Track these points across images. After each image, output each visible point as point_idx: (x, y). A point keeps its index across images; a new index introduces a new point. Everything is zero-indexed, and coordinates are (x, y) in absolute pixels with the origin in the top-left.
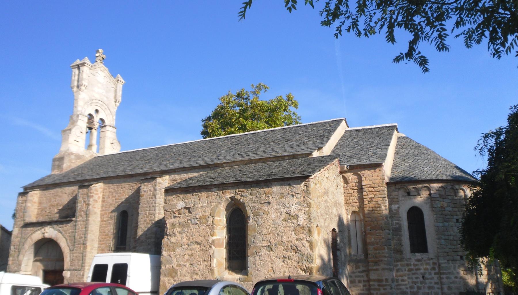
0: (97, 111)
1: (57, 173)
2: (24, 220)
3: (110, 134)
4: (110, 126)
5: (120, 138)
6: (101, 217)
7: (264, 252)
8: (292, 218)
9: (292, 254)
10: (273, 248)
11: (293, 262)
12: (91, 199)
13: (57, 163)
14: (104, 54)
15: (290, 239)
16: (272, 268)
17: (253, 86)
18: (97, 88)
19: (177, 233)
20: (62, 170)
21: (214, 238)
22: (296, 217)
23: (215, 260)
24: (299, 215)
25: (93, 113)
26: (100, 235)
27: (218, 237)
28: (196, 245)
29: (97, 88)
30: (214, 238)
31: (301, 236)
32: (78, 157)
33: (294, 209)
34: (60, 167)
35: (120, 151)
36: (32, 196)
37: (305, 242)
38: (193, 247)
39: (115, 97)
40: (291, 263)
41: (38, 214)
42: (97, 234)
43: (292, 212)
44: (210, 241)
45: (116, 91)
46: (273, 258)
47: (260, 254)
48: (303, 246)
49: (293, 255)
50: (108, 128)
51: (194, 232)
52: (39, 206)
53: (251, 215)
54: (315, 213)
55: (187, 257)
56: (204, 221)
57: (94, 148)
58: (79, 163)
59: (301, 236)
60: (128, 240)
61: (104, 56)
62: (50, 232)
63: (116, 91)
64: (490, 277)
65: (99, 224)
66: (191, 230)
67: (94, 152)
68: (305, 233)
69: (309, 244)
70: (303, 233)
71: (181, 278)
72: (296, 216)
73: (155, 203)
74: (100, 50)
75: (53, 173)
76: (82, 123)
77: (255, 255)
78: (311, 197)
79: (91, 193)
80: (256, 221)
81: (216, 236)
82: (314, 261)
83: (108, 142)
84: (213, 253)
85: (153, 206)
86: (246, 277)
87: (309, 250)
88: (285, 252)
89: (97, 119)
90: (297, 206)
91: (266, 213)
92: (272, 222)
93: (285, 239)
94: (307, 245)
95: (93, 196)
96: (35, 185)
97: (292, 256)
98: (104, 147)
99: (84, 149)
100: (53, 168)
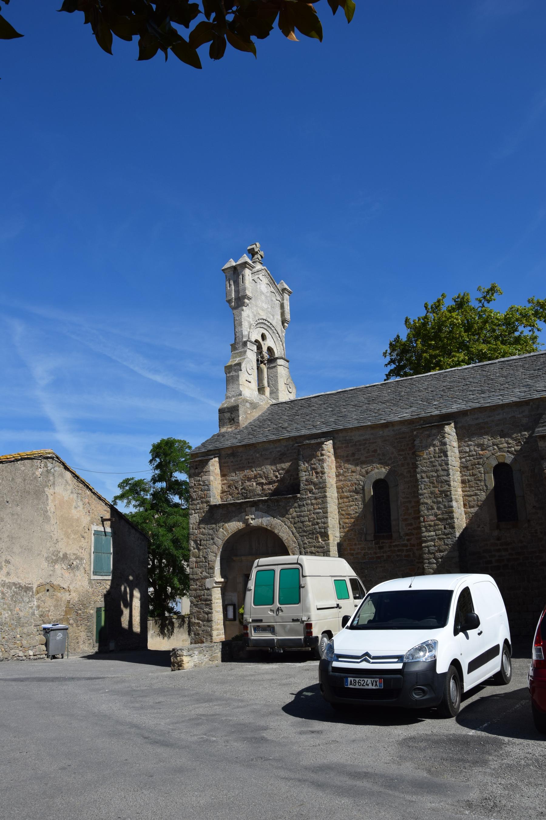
2: (208, 502)
3: (282, 370)
5: (296, 379)
6: (338, 492)
17: (479, 289)
20: (239, 426)
26: (340, 519)
35: (296, 397)
36: (213, 465)
39: (283, 314)
42: (337, 517)
45: (282, 306)
50: (280, 362)
52: (222, 480)
60: (393, 523)
61: (262, 253)
63: (282, 306)
64: (273, 463)
65: (336, 501)
73: (447, 464)
74: (258, 244)
75: (223, 430)
83: (282, 386)
85: (444, 470)
96: (210, 447)
98: (277, 390)
100: (222, 422)
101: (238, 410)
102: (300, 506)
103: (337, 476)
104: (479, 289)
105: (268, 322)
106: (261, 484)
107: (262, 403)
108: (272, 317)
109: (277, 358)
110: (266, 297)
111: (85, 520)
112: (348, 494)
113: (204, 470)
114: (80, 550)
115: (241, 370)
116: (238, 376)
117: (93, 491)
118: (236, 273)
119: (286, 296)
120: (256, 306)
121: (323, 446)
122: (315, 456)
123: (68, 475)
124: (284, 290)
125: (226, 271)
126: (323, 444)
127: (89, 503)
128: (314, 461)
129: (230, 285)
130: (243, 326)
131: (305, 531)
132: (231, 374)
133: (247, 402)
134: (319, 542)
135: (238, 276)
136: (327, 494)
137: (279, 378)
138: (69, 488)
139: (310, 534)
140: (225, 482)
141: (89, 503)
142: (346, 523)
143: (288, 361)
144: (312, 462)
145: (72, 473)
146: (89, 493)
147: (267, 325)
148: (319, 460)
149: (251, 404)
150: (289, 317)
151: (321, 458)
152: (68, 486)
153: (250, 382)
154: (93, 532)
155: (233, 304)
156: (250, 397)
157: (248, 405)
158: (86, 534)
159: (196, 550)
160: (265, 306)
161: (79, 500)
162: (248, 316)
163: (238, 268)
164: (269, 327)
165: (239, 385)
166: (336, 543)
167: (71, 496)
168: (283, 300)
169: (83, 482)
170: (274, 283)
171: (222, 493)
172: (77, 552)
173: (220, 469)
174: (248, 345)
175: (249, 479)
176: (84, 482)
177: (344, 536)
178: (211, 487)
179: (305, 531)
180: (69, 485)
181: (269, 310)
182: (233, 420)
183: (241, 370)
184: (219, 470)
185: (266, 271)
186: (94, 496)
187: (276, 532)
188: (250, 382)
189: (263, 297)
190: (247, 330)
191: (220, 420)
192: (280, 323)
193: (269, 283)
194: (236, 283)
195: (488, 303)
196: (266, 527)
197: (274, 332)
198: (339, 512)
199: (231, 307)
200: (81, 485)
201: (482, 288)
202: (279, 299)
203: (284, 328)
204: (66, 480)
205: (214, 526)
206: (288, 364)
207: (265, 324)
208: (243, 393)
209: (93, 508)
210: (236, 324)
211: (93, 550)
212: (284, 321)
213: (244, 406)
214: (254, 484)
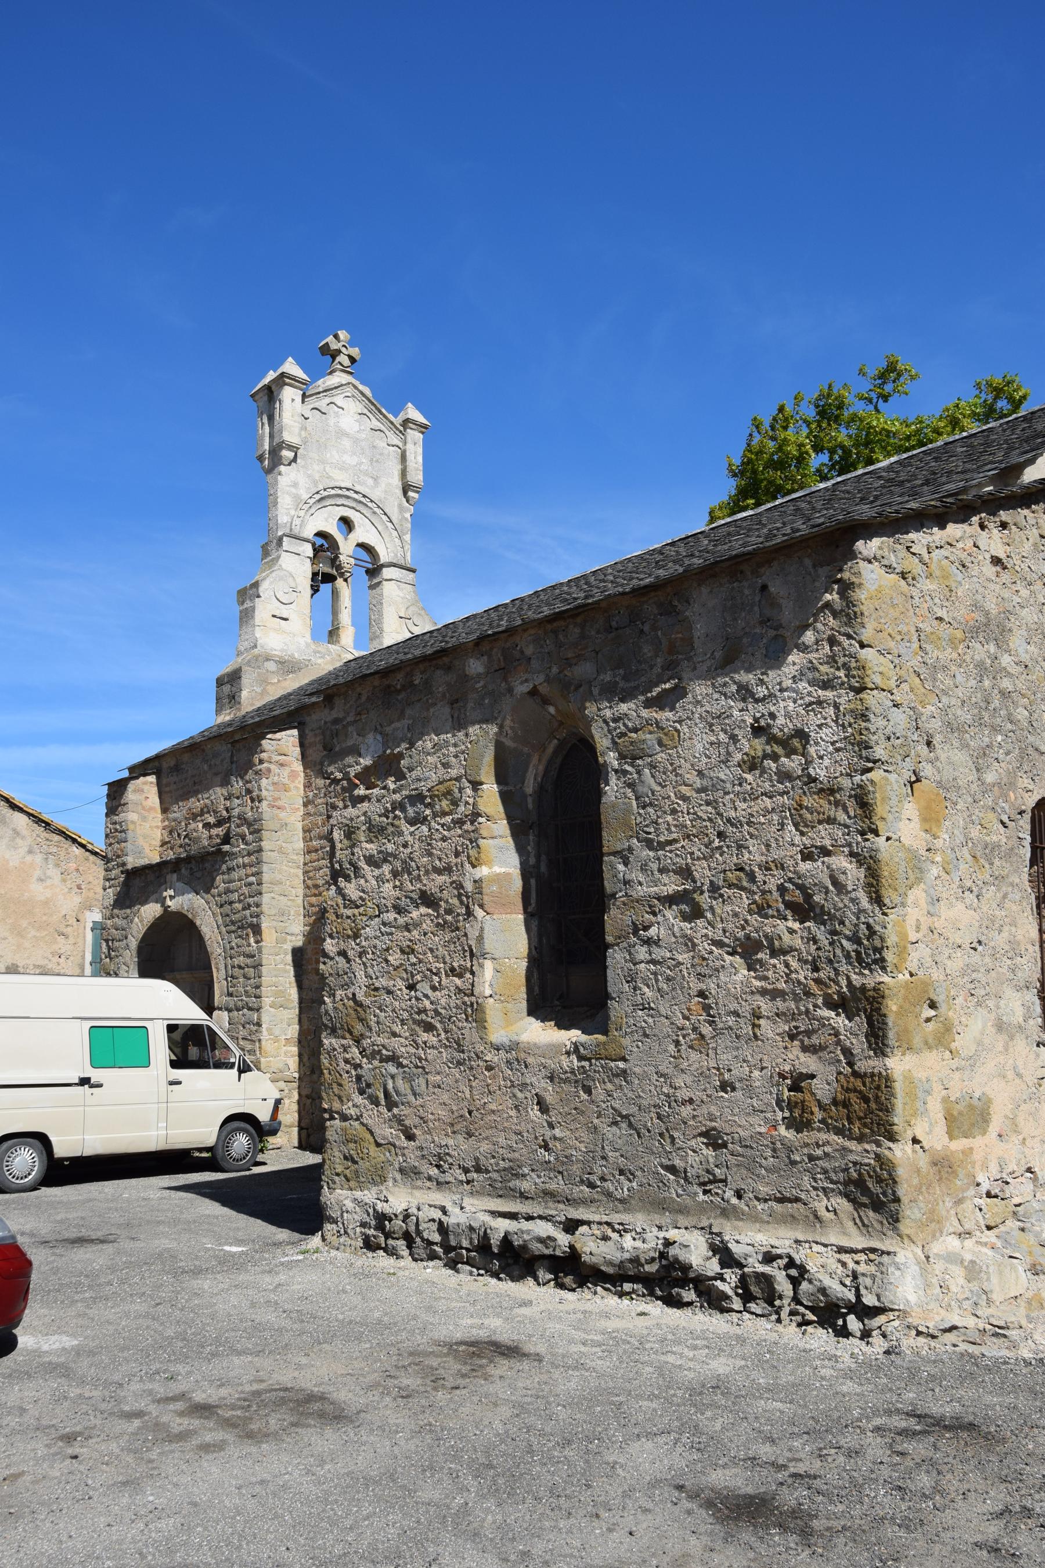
0: (347, 523)
1: (228, 718)
4: (395, 565)
7: (669, 923)
8: (779, 750)
9: (787, 930)
10: (704, 900)
11: (794, 964)
12: (264, 782)
13: (226, 689)
14: (352, 343)
15: (776, 854)
16: (701, 994)
18: (342, 448)
19: (362, 864)
20: (239, 710)
21: (483, 871)
22: (798, 740)
23: (488, 965)
24: (811, 730)
25: (332, 528)
27: (497, 869)
28: (423, 910)
29: (342, 448)
30: (483, 871)
31: (823, 835)
32: (288, 666)
33: (786, 713)
34: (233, 699)
36: (140, 791)
37: (841, 862)
38: (415, 914)
39: (404, 473)
40: (781, 967)
41: (164, 844)
43: (781, 721)
44: (469, 886)
45: (403, 458)
46: (704, 946)
47: (653, 932)
48: (835, 882)
49: (791, 931)
50: (387, 573)
51: (415, 855)
52: (163, 821)
53: (611, 758)
54: (900, 719)
55: (395, 958)
56: (445, 804)
57: (347, 636)
58: (292, 683)
59: (823, 835)
61: (355, 352)
62: (181, 901)
63: (403, 458)
66: (405, 846)
67: (349, 648)
68: (842, 817)
69: (862, 873)
70: (831, 821)
71: (380, 1040)
72: (796, 743)
74: (343, 335)
76: (296, 565)
77: (633, 939)
78: (866, 635)
79: (261, 762)
80: (631, 785)
81: (489, 864)
82: (890, 956)
84: (480, 939)
86: (601, 1038)
87: (865, 903)
88: (754, 920)
89: (347, 548)
90: (803, 686)
91: (668, 739)
92: (692, 777)
93: (754, 855)
94: (853, 873)
95: (269, 770)
97: (786, 938)
98: (382, 630)
99: (308, 638)
101: (240, 678)
102: (230, 870)
103: (305, 805)
104: (862, 373)
105: (356, 492)
106: (207, 826)
107: (319, 661)
108: (370, 482)
109: (383, 566)
110: (356, 441)
111: (69, 903)
112: (318, 842)
113: (122, 802)
114: (56, 959)
115: (259, 596)
116: (253, 608)
117: (90, 847)
118: (270, 394)
119: (415, 436)
120: (323, 462)
121: (263, 742)
122: (250, 765)
123: (21, 819)
124: (406, 422)
125: (257, 397)
126: (264, 738)
127: (77, 870)
128: (250, 775)
129: (263, 424)
130: (279, 505)
131: (233, 923)
132: (245, 606)
133: (268, 660)
134: (249, 945)
135: (275, 403)
136: (263, 844)
137: (385, 605)
138: (23, 845)
139: (239, 928)
140: (166, 823)
141: (77, 870)
142: (312, 905)
143: (414, 571)
144: (247, 777)
145: (29, 815)
146: (76, 851)
147: (355, 500)
148: (256, 773)
149: (281, 662)
150: (421, 477)
151: (259, 767)
152: (19, 841)
153: (286, 619)
154: (90, 925)
155: (266, 462)
156: (282, 650)
157: (271, 666)
158: (69, 929)
159: (108, 960)
160: (351, 460)
161: (50, 866)
162: (295, 485)
163: (274, 388)
164: (360, 502)
165: (254, 626)
166: (288, 947)
167: (29, 858)
168: (405, 443)
169: (61, 833)
170: (380, 411)
171: (162, 846)
172: (46, 962)
173: (160, 798)
174: (284, 544)
175: (194, 817)
176: (64, 833)
177: (310, 933)
178: (130, 835)
179: (233, 923)
180: (23, 838)
181: (363, 467)
182: (234, 697)
183: (259, 596)
184: (158, 800)
185: (355, 387)
186: (92, 858)
187: (198, 923)
188: (286, 619)
189: (346, 443)
190: (288, 514)
191: (218, 699)
192: (399, 492)
193: (366, 411)
194: (271, 419)
195: (886, 401)
196: (186, 913)
197: (375, 513)
198: (304, 881)
199: (263, 468)
200: (57, 838)
201: (866, 369)
202: (396, 442)
203: (408, 501)
204: (14, 830)
205: (128, 911)
206: (411, 575)
207: (348, 497)
208: (260, 642)
209: (91, 879)
210: (264, 502)
211: (89, 957)
212: (406, 489)
213: (259, 667)
214: (200, 825)
